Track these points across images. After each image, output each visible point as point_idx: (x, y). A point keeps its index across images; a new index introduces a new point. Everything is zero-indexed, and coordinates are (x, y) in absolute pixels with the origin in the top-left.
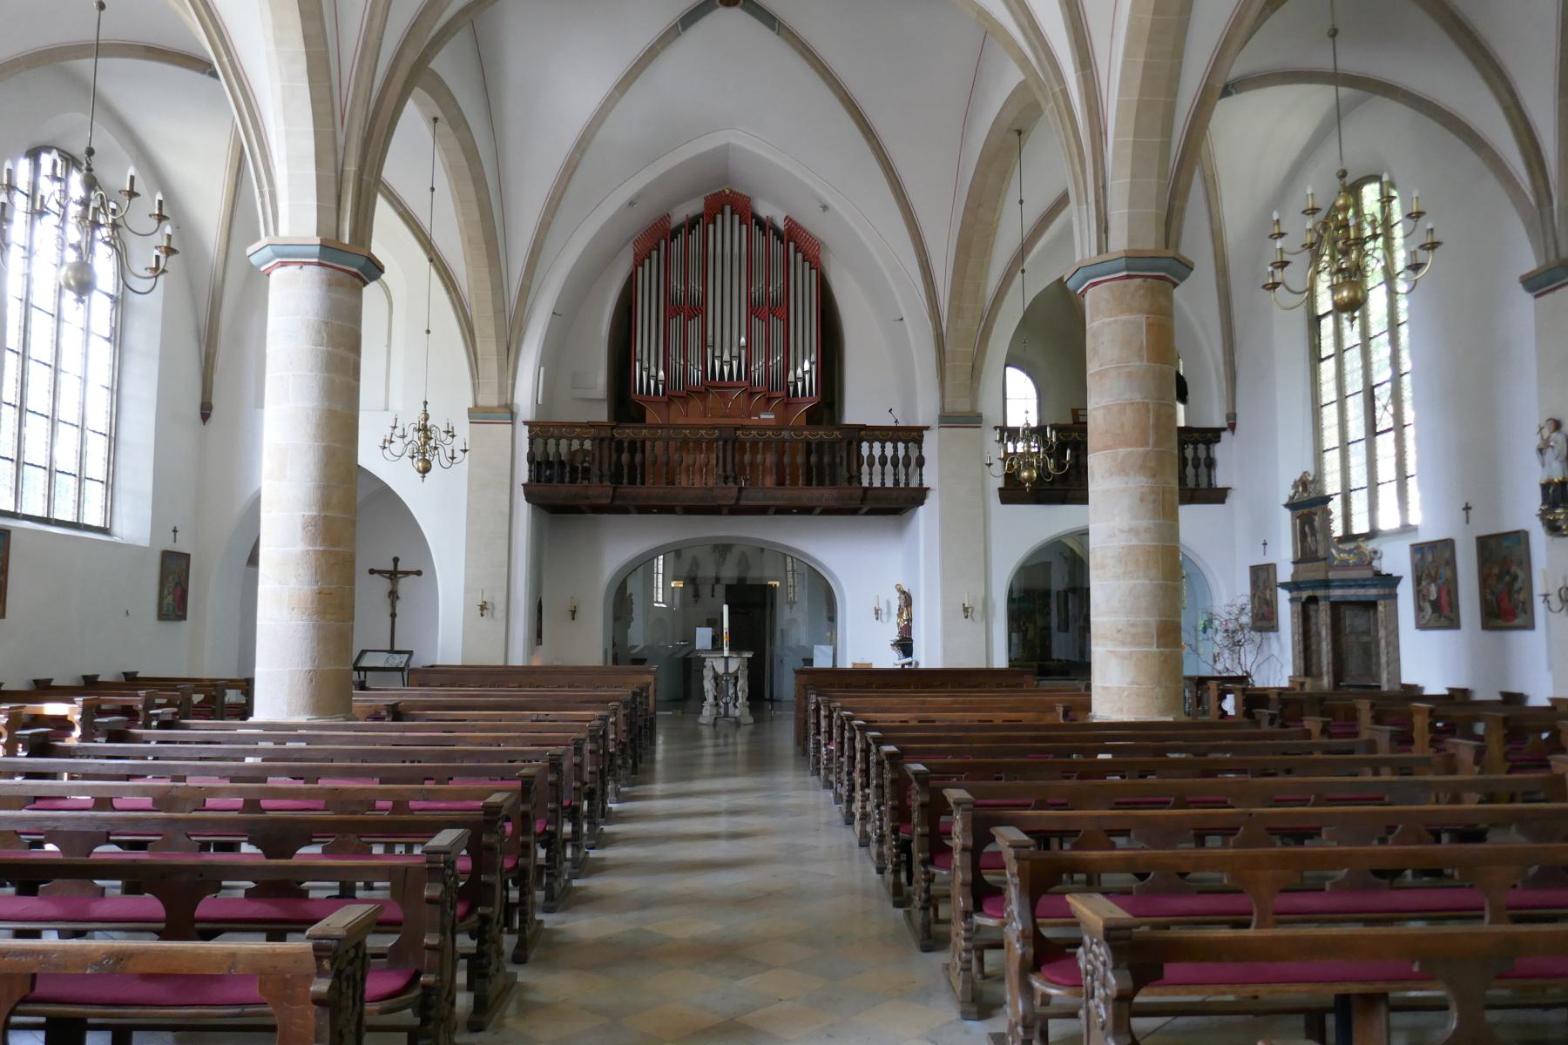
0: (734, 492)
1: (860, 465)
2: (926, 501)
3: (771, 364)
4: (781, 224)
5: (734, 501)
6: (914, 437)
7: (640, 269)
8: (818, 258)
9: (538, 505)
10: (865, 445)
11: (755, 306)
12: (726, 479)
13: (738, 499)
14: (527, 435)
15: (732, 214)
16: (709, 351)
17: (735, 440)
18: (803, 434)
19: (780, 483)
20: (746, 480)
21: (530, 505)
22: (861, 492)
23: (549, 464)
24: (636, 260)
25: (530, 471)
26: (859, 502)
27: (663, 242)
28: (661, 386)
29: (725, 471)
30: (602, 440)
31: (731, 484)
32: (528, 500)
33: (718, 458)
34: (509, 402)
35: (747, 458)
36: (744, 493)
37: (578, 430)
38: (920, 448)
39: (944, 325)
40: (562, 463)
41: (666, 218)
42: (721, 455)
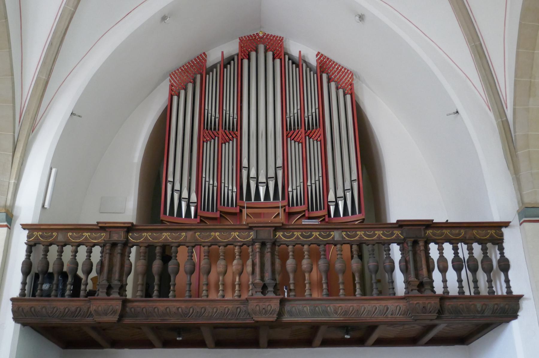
0: (275, 305)
1: (430, 271)
2: (519, 314)
3: (309, 184)
4: (313, 61)
5: (275, 316)
6: (491, 236)
7: (175, 98)
8: (351, 84)
9: (24, 325)
10: (433, 248)
11: (290, 128)
12: (264, 288)
13: (280, 314)
14: (25, 239)
15: (266, 51)
16: (245, 173)
17: (274, 243)
18: (356, 235)
19: (332, 291)
20: (290, 290)
21: (19, 326)
22: (437, 301)
23: (49, 277)
24: (171, 90)
25: (24, 283)
26: (435, 315)
27: (198, 77)
28: (193, 209)
29: (262, 278)
30: (114, 245)
31: (271, 295)
32: (16, 319)
33: (254, 265)
34: (8, 203)
35: (290, 263)
36: (288, 307)
37: (86, 234)
38: (501, 249)
39: (509, 113)
40: (64, 275)
41: (202, 58)
42: (257, 261)
